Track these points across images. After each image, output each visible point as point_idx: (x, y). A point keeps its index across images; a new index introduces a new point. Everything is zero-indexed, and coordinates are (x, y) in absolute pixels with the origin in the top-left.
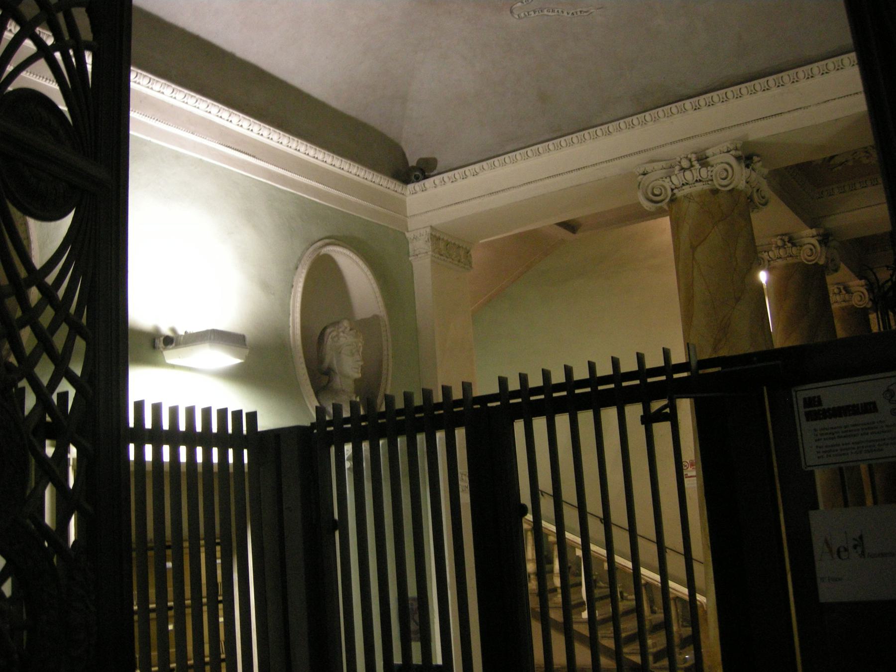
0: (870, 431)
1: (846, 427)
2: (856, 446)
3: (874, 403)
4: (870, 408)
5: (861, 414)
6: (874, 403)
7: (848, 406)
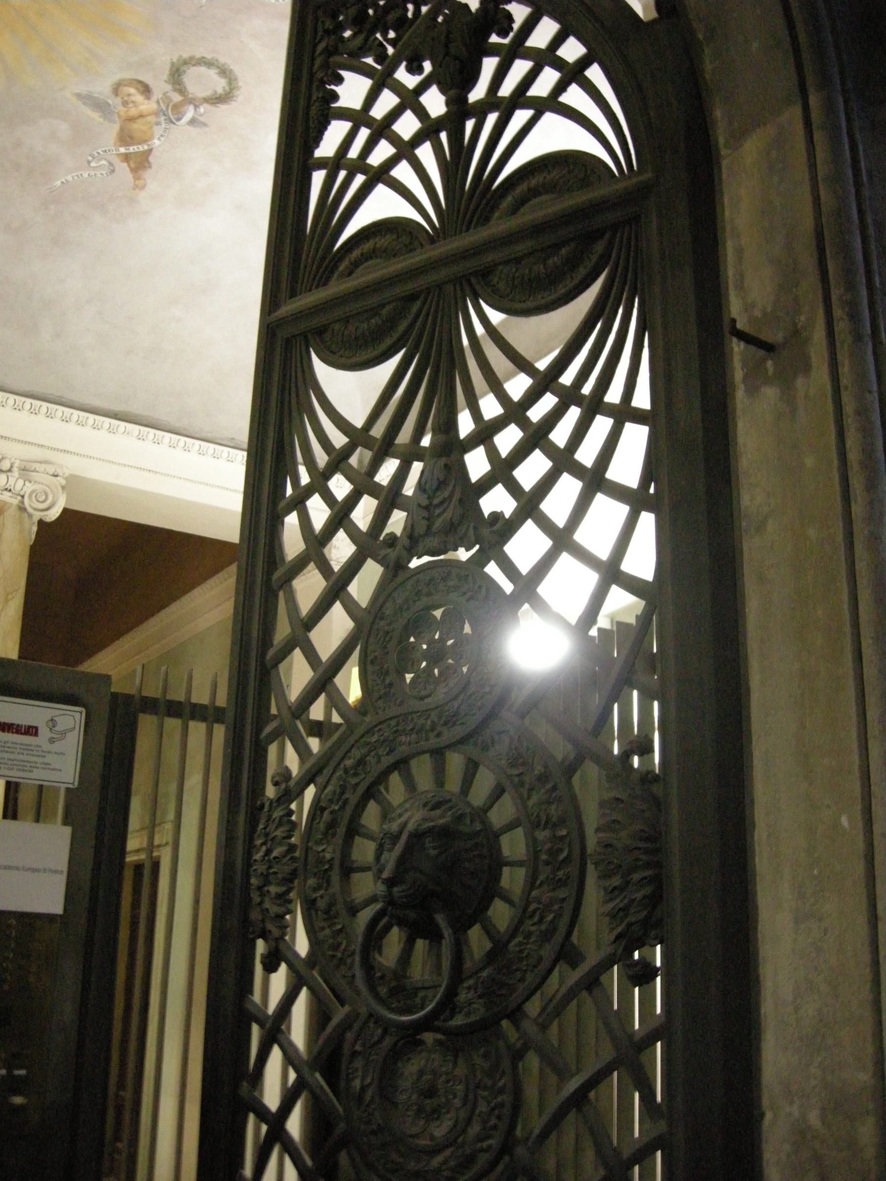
0: (25, 752)
1: (5, 742)
2: (10, 762)
3: (36, 728)
4: (32, 731)
5: (22, 734)
6: (36, 728)
7: (12, 724)
